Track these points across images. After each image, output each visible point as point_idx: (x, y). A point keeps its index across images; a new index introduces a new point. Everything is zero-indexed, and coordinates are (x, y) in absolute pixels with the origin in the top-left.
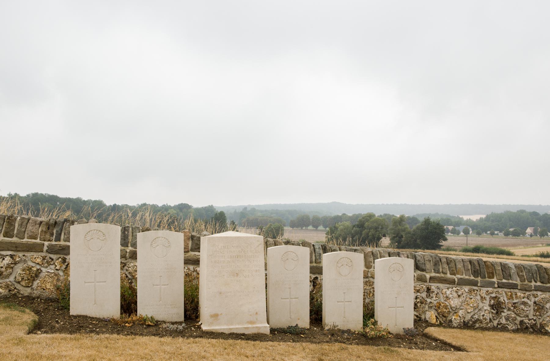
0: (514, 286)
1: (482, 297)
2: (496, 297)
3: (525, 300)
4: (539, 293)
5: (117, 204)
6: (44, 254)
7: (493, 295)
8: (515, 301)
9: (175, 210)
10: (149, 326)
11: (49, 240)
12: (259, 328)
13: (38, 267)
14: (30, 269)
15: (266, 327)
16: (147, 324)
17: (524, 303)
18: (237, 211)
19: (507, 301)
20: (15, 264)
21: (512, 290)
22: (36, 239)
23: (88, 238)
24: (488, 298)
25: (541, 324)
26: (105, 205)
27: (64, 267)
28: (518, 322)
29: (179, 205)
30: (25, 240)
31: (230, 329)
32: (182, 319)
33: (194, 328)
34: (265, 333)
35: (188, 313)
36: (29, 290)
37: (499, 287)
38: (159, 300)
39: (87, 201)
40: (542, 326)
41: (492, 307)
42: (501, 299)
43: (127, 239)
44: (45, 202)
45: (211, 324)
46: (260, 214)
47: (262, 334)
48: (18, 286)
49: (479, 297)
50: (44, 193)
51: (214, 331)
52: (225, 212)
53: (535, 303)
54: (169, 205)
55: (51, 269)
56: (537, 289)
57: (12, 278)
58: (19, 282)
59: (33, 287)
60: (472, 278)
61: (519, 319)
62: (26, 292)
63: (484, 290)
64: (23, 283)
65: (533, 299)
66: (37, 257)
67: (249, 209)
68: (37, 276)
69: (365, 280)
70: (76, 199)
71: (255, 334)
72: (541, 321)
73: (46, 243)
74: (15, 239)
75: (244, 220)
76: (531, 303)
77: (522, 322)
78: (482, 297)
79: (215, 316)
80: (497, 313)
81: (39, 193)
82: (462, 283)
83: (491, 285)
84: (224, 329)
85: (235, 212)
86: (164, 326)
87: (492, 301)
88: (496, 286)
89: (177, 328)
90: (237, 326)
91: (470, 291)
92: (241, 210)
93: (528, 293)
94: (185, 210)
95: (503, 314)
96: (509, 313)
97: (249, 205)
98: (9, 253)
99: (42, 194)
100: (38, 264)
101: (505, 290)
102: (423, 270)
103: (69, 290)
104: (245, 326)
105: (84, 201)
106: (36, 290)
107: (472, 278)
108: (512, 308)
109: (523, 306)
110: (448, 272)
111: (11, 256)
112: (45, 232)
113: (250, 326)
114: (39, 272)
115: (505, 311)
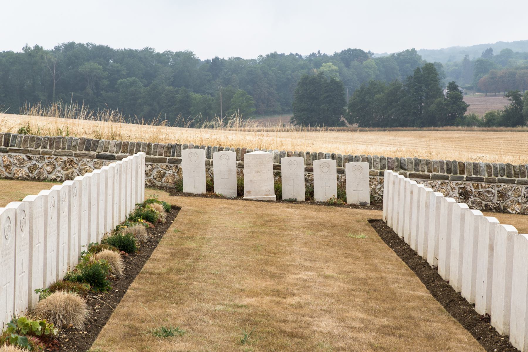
0: (481, 180)
1: (452, 187)
2: (464, 188)
3: (490, 189)
4: (503, 184)
5: (221, 57)
6: (167, 164)
7: (462, 186)
8: (481, 190)
9: (334, 64)
11: (169, 156)
12: (271, 198)
14: (160, 172)
17: (488, 192)
19: (473, 190)
20: (153, 169)
21: (479, 182)
22: (162, 155)
24: (457, 188)
25: (504, 207)
26: (198, 61)
27: (177, 170)
28: (483, 205)
29: (344, 53)
30: (157, 156)
36: (160, 183)
37: (467, 180)
38: (224, 185)
39: (163, 54)
40: (505, 208)
41: (461, 194)
42: (469, 189)
43: (209, 156)
44: (88, 60)
45: (247, 196)
46: (521, 62)
48: (155, 181)
49: (449, 188)
50: (84, 42)
53: (498, 191)
54: (322, 53)
55: (171, 172)
56: (500, 181)
57: (152, 177)
58: (155, 179)
60: (446, 174)
61: (484, 203)
62: (159, 184)
63: (454, 183)
64: (157, 179)
65: (497, 189)
66: (164, 165)
68: (164, 175)
69: (276, 171)
70: (143, 51)
72: (504, 204)
73: (168, 158)
74: (152, 156)
75: (485, 77)
76: (495, 191)
77: (486, 205)
78: (452, 187)
80: (465, 198)
81: (77, 42)
82: (435, 178)
83: (461, 179)
87: (461, 190)
88: (465, 179)
91: (442, 184)
92: (479, 56)
93: (493, 184)
94: (355, 63)
95: (470, 199)
96: (476, 198)
97: (500, 43)
98: (150, 163)
99: (81, 45)
101: (473, 182)
102: (405, 170)
103: (182, 182)
105: (158, 54)
107: (446, 174)
108: (477, 195)
109: (487, 194)
110: (426, 170)
111: (151, 165)
112: (167, 152)
114: (165, 173)
115: (472, 197)
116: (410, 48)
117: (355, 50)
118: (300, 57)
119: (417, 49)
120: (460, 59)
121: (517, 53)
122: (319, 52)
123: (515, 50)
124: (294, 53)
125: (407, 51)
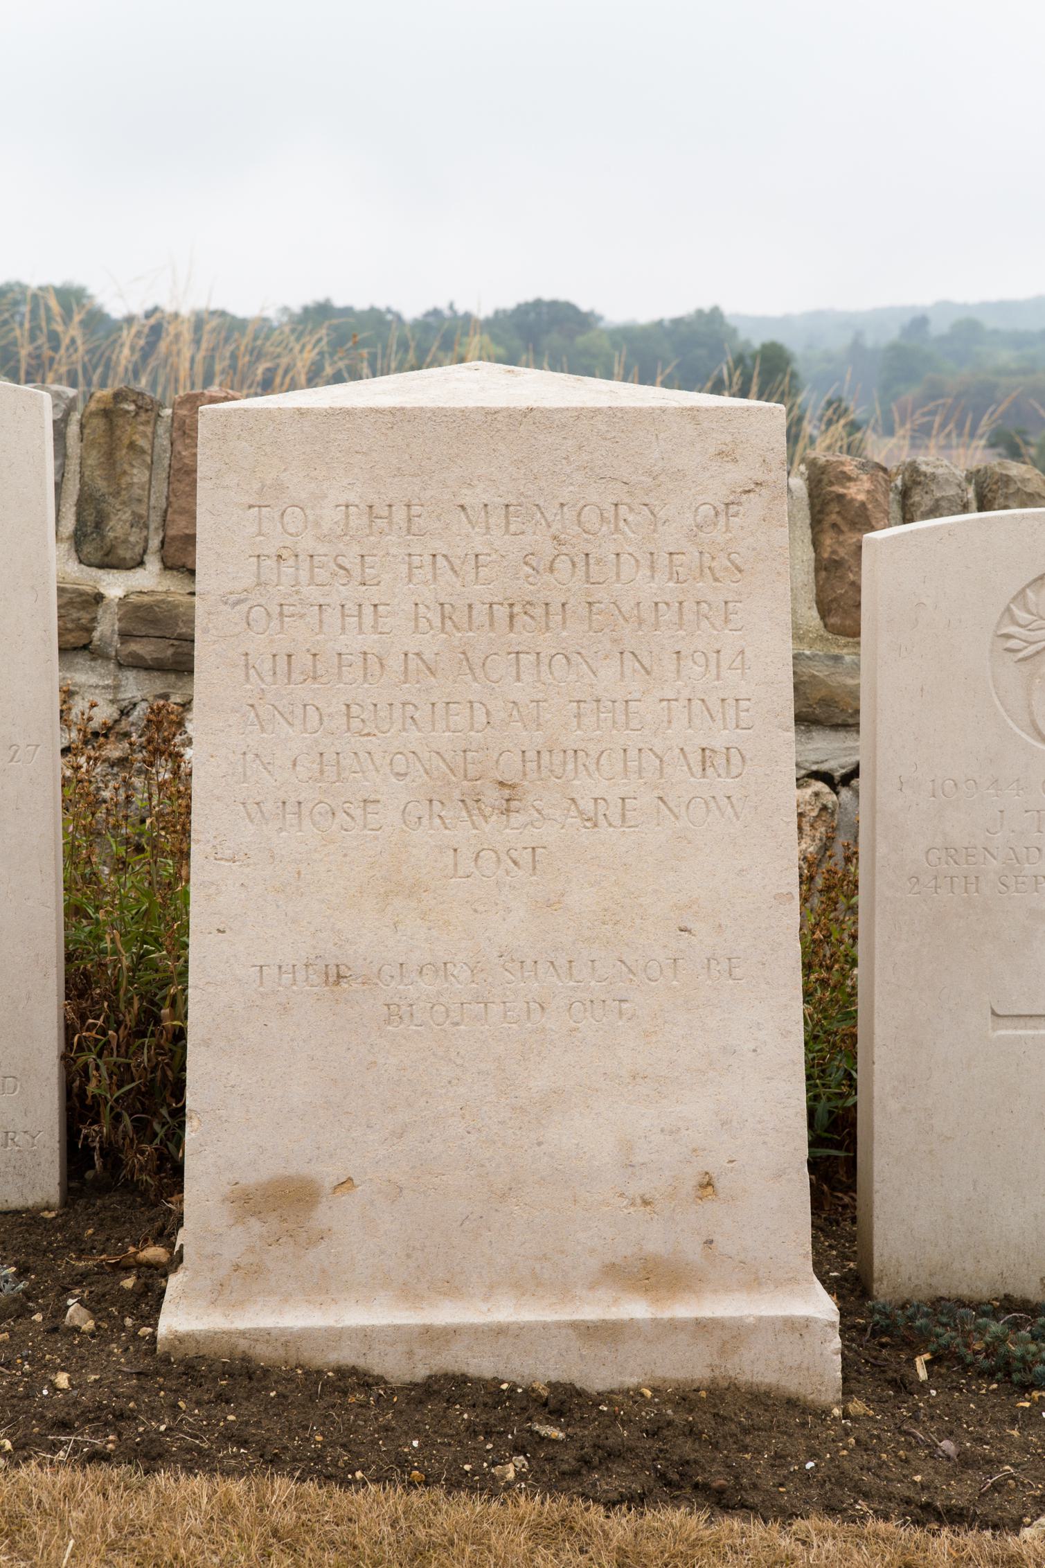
12: (729, 1335)
15: (798, 1327)
18: (869, 341)
31: (431, 1336)
33: (93, 1305)
34: (792, 1385)
35: (96, 1133)
45: (246, 1278)
47: (760, 1398)
51: (264, 1353)
52: (794, 344)
54: (461, 309)
67: (939, 327)
71: (685, 1398)
79: (285, 1203)
84: (366, 1335)
85: (856, 347)
90: (505, 1312)
92: (892, 334)
97: (944, 306)
104: (591, 1311)
113: (636, 1309)
116: (706, 306)
117: (554, 304)
118: (398, 317)
119: (728, 309)
120: (839, 343)
121: (995, 332)
122: (451, 307)
123: (990, 323)
124: (381, 305)
125: (700, 313)
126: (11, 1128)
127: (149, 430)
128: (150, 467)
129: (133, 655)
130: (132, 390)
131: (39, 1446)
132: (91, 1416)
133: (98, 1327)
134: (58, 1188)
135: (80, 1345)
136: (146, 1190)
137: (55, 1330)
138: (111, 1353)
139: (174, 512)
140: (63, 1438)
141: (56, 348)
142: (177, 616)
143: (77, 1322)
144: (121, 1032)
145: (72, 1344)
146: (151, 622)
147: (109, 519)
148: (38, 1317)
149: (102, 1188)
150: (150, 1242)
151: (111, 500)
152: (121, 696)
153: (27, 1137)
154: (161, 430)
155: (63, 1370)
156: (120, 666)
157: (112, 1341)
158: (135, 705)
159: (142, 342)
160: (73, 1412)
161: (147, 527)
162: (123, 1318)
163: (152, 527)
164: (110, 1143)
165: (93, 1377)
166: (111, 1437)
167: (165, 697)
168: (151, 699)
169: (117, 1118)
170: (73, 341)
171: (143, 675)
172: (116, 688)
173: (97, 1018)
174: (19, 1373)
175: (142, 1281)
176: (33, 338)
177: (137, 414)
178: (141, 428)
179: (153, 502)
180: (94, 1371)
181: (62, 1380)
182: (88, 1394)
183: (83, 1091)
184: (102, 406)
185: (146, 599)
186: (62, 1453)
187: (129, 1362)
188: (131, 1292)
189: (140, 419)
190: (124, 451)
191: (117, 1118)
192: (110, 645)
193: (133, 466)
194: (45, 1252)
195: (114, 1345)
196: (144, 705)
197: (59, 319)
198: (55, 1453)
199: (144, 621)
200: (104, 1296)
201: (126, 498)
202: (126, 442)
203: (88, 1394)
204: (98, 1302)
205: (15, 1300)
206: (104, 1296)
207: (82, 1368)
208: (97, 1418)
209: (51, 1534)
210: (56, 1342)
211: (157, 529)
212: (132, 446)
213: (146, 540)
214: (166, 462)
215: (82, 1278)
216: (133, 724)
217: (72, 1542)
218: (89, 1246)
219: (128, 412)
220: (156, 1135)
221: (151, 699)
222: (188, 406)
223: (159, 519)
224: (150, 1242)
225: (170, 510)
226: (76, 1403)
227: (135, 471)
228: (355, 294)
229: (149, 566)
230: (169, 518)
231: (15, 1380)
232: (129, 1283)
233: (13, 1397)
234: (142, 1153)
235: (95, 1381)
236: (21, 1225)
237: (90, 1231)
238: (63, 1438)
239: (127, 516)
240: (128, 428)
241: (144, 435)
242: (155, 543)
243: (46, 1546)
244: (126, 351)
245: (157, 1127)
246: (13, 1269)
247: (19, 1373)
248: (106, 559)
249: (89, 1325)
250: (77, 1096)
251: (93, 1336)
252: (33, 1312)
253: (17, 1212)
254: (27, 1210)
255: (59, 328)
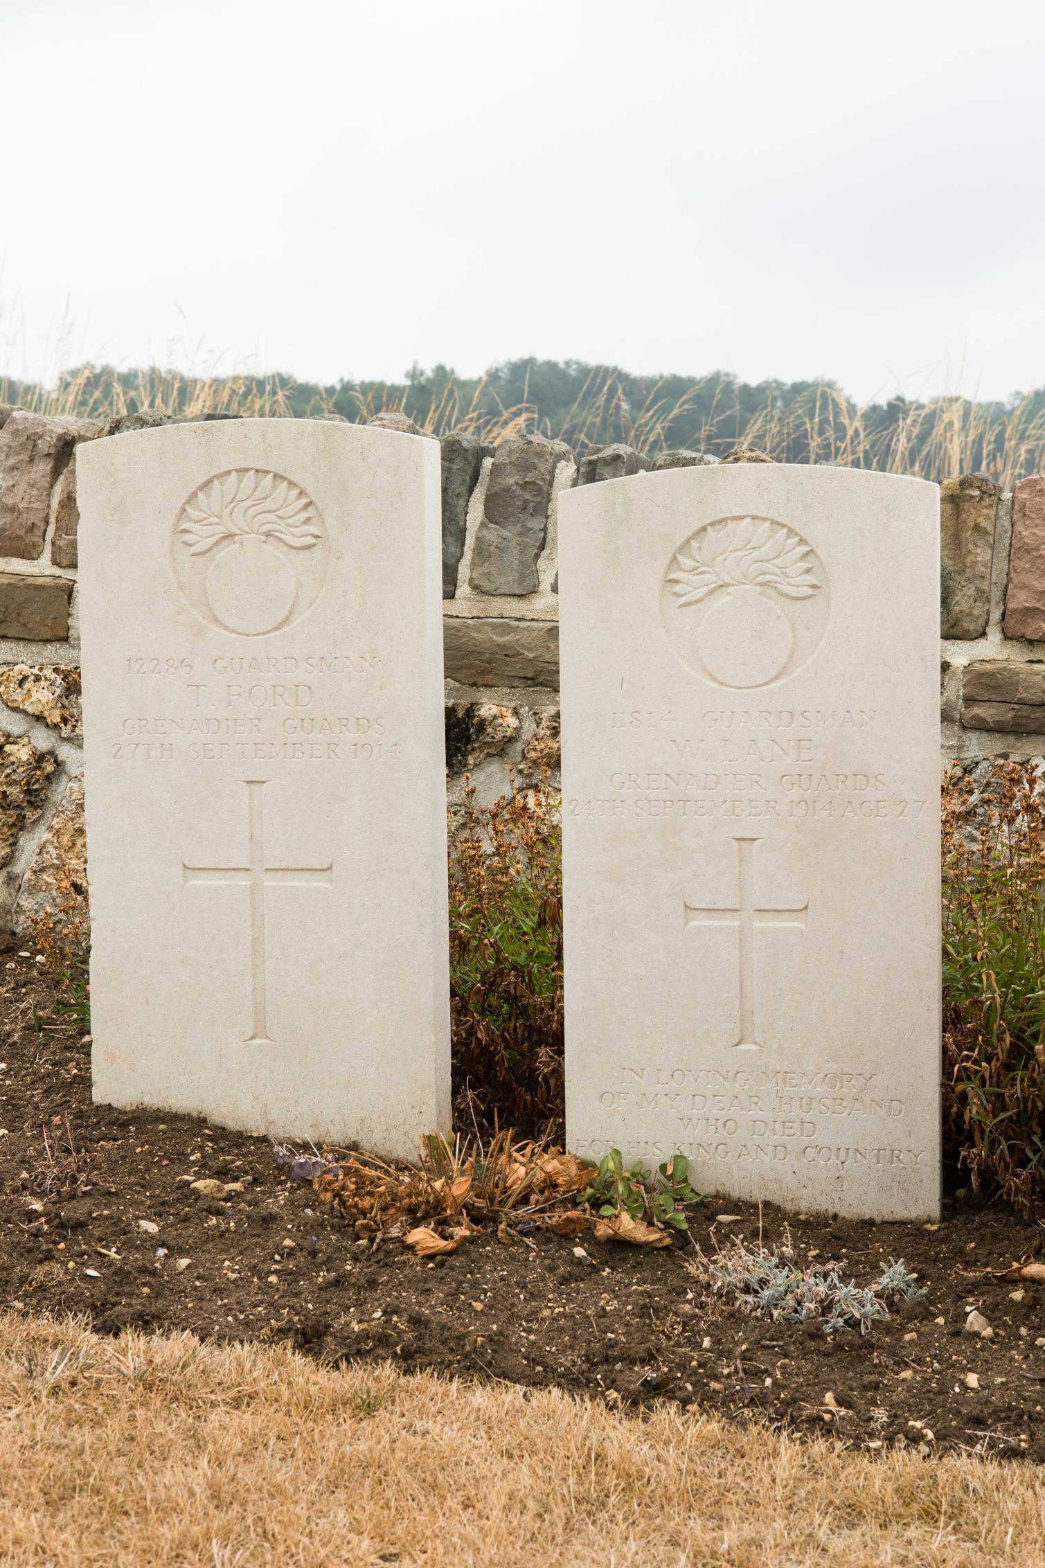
10: (619, 1247)
13: (42, 740)
16: (602, 1230)
22: (28, 552)
23: (202, 537)
32: (924, 1200)
33: (990, 1313)
35: (976, 1154)
39: (761, 389)
50: (560, 358)
59: (17, 868)
81: (541, 357)
86: (738, 1264)
89: (826, 1306)
99: (552, 366)
100: (39, 718)
105: (745, 389)
106: (33, 889)
126: (897, 1147)
127: (992, 512)
128: (992, 548)
129: (976, 718)
130: (976, 477)
131: (958, 1438)
132: (1003, 1415)
133: (997, 1334)
134: (938, 1204)
135: (983, 1349)
136: (1021, 1211)
137: (957, 1333)
138: (1012, 1359)
139: (1015, 587)
140: (979, 1433)
141: (842, 439)
142: (1018, 682)
143: (976, 1328)
144: (993, 1063)
145: (974, 1347)
146: (994, 687)
147: (954, 593)
148: (940, 1320)
149: (975, 1206)
150: (1032, 1259)
151: (957, 577)
152: (964, 755)
153: (911, 1155)
154: (1002, 513)
155: (970, 1370)
156: (964, 728)
157: (1012, 1348)
158: (977, 764)
159: (916, 431)
160: (986, 1410)
161: (988, 600)
162: (1018, 1327)
163: (994, 600)
164: (987, 1166)
165: (999, 1380)
166: (1023, 1437)
167: (1005, 756)
168: (992, 758)
169: (993, 1144)
170: (857, 433)
171: (985, 735)
172: (960, 748)
173: (972, 1049)
174: (930, 1370)
175: (1031, 1294)
176: (821, 432)
177: (981, 499)
178: (985, 511)
179: (994, 578)
180: (1000, 1374)
181: (972, 1380)
182: (997, 1394)
183: (960, 1115)
184: (950, 493)
185: (989, 667)
186: (979, 1446)
187: (1030, 1369)
188: (1022, 1304)
189: (983, 503)
190: (969, 533)
191: (993, 1144)
192: (955, 709)
193: (977, 546)
194: (935, 1261)
195: (1014, 1352)
196: (986, 763)
197: (845, 413)
198: (973, 1447)
199: (988, 687)
200: (997, 1305)
201: (970, 575)
202: (971, 524)
203: (997, 1394)
204: (993, 1311)
205: (919, 1304)
206: (997, 1305)
207: (987, 1370)
208: (1008, 1418)
209: (992, 1522)
210: (960, 1344)
211: (998, 603)
212: (977, 528)
213: (988, 613)
214: (1007, 542)
215: (973, 1288)
216: (975, 781)
217: (1011, 1530)
218: (973, 1259)
219: (973, 497)
220: (1030, 1161)
221: (992, 758)
222: (1028, 490)
223: (1000, 594)
224: (1032, 1259)
225: (1011, 586)
226: (988, 1402)
227: (979, 551)
228: (128, 354)
229: (990, 637)
230: (1009, 592)
231: (927, 1376)
232: (1018, 1295)
233: (929, 1391)
234: (1018, 1176)
235: (1002, 1383)
236: (907, 1235)
237: (972, 1245)
238: (979, 1433)
239: (971, 591)
240: (973, 511)
241: (987, 517)
242: (995, 616)
243: (989, 1531)
244: (903, 439)
245: (1029, 1153)
246: (915, 1275)
247: (930, 1370)
248: (952, 631)
249: (988, 1332)
250: (954, 1121)
251: (993, 1343)
252: (935, 1316)
253: (902, 1223)
254: (911, 1222)
255: (846, 421)
